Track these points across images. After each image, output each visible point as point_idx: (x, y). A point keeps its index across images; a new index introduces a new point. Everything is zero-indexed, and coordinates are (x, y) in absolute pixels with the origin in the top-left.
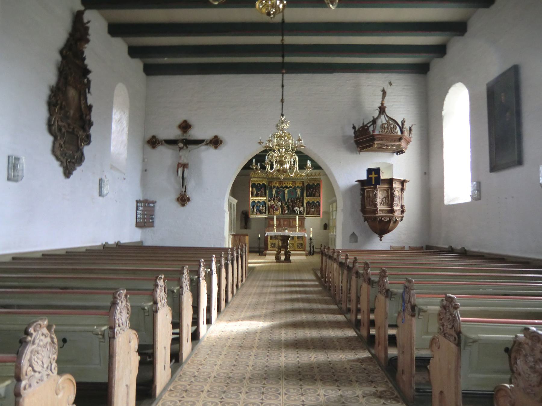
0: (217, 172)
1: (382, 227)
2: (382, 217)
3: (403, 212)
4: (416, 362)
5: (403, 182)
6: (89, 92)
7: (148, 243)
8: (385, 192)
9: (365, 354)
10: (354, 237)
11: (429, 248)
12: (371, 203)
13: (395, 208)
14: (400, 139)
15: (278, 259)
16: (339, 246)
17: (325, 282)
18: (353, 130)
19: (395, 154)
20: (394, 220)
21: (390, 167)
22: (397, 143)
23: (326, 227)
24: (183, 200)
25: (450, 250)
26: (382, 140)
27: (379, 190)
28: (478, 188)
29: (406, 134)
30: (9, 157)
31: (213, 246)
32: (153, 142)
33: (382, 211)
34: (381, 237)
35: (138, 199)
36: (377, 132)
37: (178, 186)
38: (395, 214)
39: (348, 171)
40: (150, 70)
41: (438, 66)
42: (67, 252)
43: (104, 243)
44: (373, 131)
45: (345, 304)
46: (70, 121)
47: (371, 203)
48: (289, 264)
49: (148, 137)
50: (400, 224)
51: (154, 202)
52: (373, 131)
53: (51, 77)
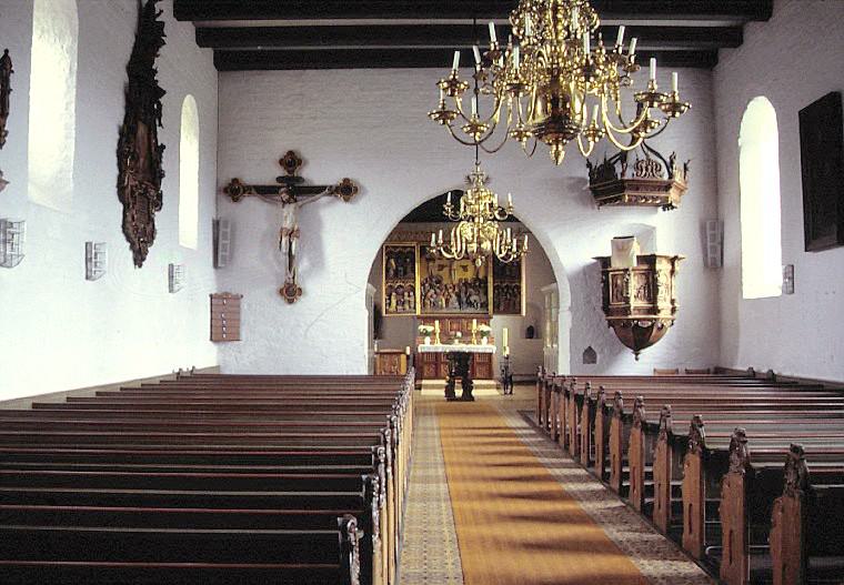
0: (349, 243)
1: (639, 338)
2: (638, 320)
3: (673, 310)
4: (682, 520)
5: (673, 260)
6: (160, 125)
7: (233, 369)
8: (644, 277)
9: (619, 504)
10: (590, 355)
11: (718, 370)
12: (619, 296)
13: (660, 304)
14: (667, 187)
15: (450, 391)
16: (564, 368)
17: (549, 429)
18: (588, 170)
19: (660, 209)
20: (660, 325)
21: (649, 233)
22: (663, 195)
23: (531, 333)
24: (291, 292)
25: (751, 373)
26: (637, 189)
27: (632, 274)
28: (790, 273)
29: (678, 178)
30: (87, 244)
31: (345, 374)
32: (234, 190)
33: (638, 309)
34: (637, 354)
35: (213, 292)
36: (628, 176)
37: (283, 269)
38: (661, 315)
39: (579, 243)
40: (224, 63)
41: (731, 63)
42: (121, 389)
43: (177, 371)
44: (623, 174)
45: (586, 454)
46: (140, 176)
47: (619, 296)
48: (472, 403)
49: (226, 179)
50: (669, 332)
51: (238, 298)
52: (623, 174)
53: (118, 114)
